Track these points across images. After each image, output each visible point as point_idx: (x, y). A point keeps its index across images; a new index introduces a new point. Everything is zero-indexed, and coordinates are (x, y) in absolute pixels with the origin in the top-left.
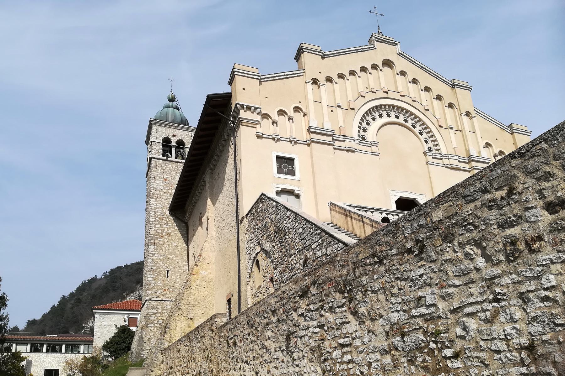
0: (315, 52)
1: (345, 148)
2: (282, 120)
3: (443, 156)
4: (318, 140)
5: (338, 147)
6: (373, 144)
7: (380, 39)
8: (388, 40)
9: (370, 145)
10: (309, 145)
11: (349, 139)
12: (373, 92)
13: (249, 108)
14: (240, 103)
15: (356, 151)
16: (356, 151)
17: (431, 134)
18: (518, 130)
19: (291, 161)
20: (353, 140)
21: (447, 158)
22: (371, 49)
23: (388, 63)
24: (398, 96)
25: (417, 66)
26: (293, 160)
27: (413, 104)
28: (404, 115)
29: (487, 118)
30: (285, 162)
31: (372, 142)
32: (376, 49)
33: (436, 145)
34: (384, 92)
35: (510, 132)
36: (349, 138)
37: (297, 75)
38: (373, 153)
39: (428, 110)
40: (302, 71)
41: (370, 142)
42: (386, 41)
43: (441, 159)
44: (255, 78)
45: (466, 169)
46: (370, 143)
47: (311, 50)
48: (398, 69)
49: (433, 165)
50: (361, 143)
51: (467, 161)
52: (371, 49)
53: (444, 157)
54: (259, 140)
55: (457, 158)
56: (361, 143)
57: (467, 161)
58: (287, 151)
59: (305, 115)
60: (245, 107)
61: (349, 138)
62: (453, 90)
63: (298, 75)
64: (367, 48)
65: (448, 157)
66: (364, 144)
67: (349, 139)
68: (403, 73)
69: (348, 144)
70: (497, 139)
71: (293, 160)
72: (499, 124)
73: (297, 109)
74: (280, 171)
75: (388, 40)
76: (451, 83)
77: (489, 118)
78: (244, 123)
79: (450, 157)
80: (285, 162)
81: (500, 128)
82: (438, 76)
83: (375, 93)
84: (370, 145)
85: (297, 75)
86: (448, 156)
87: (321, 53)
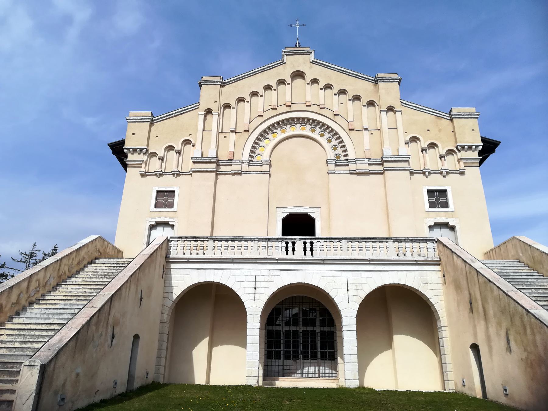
0: (213, 83)
1: (231, 172)
2: (172, 155)
3: (348, 162)
4: (206, 170)
5: (223, 172)
6: (263, 163)
7: (291, 52)
8: (300, 51)
9: (261, 164)
10: (191, 175)
11: (236, 162)
12: (273, 109)
13: (135, 150)
14: (126, 147)
15: (242, 173)
16: (242, 173)
17: (340, 140)
18: (458, 115)
19: (443, 193)
20: (241, 162)
21: (355, 163)
22: (280, 64)
23: (298, 75)
24: (304, 108)
25: (333, 70)
26: (445, 191)
27: (322, 112)
28: (311, 125)
29: (418, 108)
30: (437, 195)
31: (262, 161)
32: (285, 63)
33: (346, 151)
34: (287, 106)
35: (449, 118)
36: (237, 161)
37: (191, 109)
38: (351, 172)
39: (338, 115)
40: (197, 104)
41: (261, 161)
42: (298, 53)
43: (348, 165)
44: (146, 122)
45: (376, 171)
46: (261, 162)
47: (209, 82)
48: (308, 78)
49: (335, 173)
50: (251, 163)
51: (381, 163)
52: (278, 65)
53: (351, 163)
54: (143, 179)
55: (366, 161)
56: (251, 163)
57: (381, 163)
58: (437, 183)
59: (194, 146)
60: (131, 150)
61: (237, 161)
62: (375, 86)
63: (193, 108)
64: (274, 65)
65: (355, 162)
66: (255, 164)
67: (236, 162)
68: (315, 81)
69: (236, 167)
70: (428, 130)
71: (445, 191)
72: (435, 112)
73: (187, 142)
74: (432, 205)
75: (300, 51)
76: (373, 79)
77: (420, 108)
78: (130, 165)
79: (356, 162)
80: (166, 194)
81: (436, 116)
82: (357, 75)
83: (276, 109)
84: (261, 164)
85: (191, 109)
86: (355, 161)
87: (219, 82)
